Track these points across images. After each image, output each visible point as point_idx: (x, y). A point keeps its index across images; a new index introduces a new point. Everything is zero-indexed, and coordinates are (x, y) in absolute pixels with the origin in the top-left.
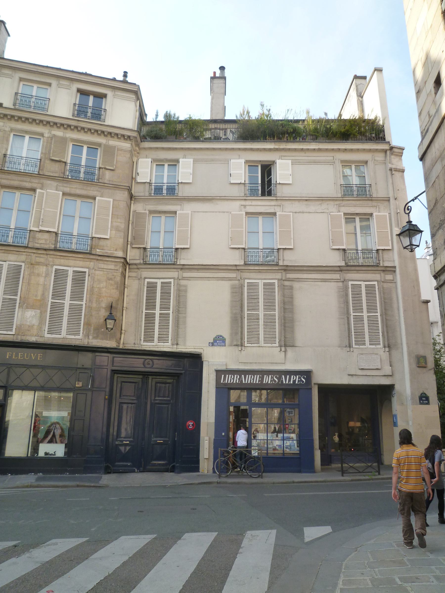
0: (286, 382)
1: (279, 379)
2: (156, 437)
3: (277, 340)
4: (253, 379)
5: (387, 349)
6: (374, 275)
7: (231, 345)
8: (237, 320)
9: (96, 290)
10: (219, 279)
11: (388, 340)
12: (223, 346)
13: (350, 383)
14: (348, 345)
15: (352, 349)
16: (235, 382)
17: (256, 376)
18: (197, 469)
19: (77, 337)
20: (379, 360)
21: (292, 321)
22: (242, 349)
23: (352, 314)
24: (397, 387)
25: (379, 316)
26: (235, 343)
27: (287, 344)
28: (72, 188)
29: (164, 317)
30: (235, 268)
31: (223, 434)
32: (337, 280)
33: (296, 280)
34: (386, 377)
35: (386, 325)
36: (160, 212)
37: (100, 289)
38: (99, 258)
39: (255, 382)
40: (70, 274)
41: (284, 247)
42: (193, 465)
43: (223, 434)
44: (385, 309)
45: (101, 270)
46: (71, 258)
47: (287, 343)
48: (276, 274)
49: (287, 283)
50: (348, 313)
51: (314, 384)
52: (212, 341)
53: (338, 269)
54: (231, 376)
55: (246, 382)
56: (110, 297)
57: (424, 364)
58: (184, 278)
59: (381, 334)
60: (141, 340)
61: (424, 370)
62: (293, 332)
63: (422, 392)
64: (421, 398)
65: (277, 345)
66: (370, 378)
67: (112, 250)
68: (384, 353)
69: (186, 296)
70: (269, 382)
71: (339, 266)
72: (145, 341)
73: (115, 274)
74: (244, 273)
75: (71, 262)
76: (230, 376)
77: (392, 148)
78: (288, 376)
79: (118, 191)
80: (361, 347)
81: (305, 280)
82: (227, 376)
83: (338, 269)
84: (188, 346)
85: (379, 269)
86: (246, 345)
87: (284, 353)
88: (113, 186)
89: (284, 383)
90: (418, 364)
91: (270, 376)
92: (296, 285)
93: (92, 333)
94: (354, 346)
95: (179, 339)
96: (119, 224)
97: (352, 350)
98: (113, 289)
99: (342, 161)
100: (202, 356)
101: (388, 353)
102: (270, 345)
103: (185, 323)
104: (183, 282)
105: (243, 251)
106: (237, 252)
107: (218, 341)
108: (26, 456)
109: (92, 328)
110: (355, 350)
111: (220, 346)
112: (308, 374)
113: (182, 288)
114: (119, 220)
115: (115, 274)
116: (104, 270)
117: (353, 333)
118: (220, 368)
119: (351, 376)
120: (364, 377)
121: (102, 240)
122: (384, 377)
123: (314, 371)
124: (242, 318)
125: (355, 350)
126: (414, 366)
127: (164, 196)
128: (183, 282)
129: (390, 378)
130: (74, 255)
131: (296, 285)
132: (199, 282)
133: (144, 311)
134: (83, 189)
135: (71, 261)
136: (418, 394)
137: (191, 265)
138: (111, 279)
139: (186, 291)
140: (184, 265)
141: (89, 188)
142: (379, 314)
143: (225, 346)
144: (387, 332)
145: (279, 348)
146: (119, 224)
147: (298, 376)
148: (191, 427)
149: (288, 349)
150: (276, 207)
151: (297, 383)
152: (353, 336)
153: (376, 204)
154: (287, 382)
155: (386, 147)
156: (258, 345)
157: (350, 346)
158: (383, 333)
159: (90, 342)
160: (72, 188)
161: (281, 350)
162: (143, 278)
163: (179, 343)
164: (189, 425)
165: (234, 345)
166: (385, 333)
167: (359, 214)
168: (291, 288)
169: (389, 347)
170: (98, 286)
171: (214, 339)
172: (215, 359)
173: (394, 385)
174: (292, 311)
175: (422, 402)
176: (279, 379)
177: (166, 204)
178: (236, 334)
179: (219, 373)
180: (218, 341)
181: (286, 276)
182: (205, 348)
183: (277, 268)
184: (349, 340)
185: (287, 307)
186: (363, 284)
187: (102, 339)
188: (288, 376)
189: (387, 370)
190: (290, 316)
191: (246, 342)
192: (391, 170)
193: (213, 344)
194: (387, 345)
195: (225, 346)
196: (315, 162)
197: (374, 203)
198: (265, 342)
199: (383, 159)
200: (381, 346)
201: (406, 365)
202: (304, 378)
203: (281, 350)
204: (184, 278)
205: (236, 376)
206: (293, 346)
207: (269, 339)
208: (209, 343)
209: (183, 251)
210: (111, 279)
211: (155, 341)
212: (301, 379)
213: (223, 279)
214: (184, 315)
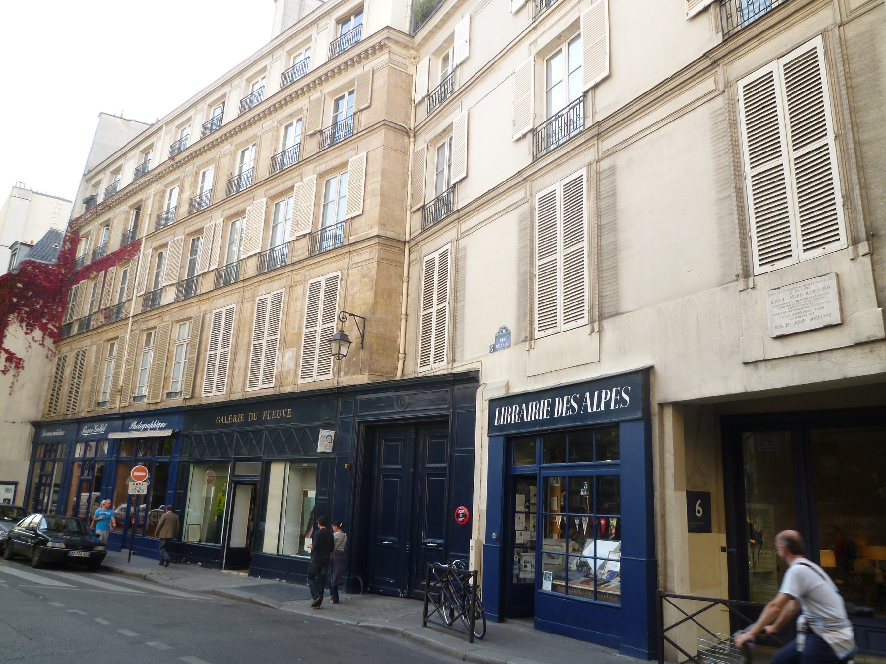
0: (592, 409)
1: (580, 402)
2: (429, 537)
6: (811, 20)
13: (749, 390)
21: (615, 250)
34: (867, 349)
38: (352, 249)
41: (592, 84)
50: (738, 174)
51: (662, 406)
53: (707, 62)
66: (812, 362)
68: (852, 264)
75: (318, 270)
78: (596, 393)
79: (374, 136)
80: (778, 265)
83: (707, 62)
91: (565, 398)
94: (758, 270)
108: (275, 553)
119: (751, 367)
121: (356, 219)
122: (859, 351)
123: (657, 368)
147: (614, 390)
148: (462, 519)
151: (612, 407)
152: (755, 240)
154: (594, 410)
157: (747, 273)
173: (478, 372)
176: (580, 402)
187: (354, 374)
188: (596, 393)
193: (494, 349)
202: (626, 392)
203: (592, 331)
206: (617, 314)
212: (621, 396)
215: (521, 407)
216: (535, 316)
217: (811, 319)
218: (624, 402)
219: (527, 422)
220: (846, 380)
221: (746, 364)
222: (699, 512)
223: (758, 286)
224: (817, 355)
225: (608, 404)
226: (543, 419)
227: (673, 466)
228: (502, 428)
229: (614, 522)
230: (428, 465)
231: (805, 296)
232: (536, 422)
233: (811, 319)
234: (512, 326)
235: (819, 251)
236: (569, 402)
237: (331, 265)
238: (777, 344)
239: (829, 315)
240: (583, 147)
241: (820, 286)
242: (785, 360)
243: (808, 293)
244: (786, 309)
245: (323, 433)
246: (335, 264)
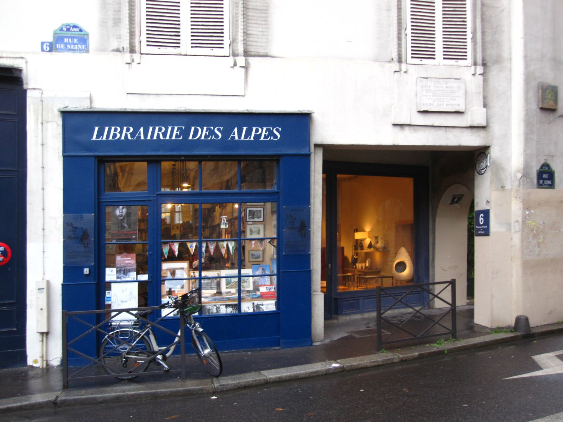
5: (480, 69)
7: (102, 50)
11: (484, 50)
12: (81, 51)
14: (395, 57)
15: (404, 67)
20: (462, 92)
22: (133, 61)
24: (494, 153)
31: (86, 271)
34: (474, 130)
35: (483, 15)
43: (86, 271)
51: (316, 146)
52: (50, 39)
57: (552, 103)
59: (469, 36)
61: (551, 116)
63: (542, 162)
64: (540, 175)
65: (226, 51)
66: (441, 132)
68: (473, 77)
82: (107, 128)
90: (543, 102)
97: (404, 69)
100: (24, 75)
101: (481, 77)
102: (208, 51)
107: (69, 38)
111: (74, 50)
112: (487, 233)
118: (73, 106)
119: (398, 128)
120: (428, 130)
123: (315, 116)
129: (482, 133)
136: (535, 168)
143: (88, 51)
144: (483, 33)
149: (251, 60)
152: (409, 38)
158: (474, 32)
161: (235, 64)
165: (113, 50)
166: (479, 34)
169: (484, 65)
171: (55, 34)
175: (541, 182)
176: (227, 132)
179: (76, 122)
180: (69, 38)
184: (399, 45)
189: (477, 116)
193: (52, 48)
194: (479, 61)
195: (88, 51)
196: (95, 205)
198: (195, 44)
203: (235, 64)
208: (43, 43)
217: (447, 105)
219: (145, 141)
220: (460, 147)
221: (395, 125)
222: (481, 221)
223: (409, 72)
224: (444, 128)
226: (170, 141)
227: (321, 196)
231: (445, 89)
233: (447, 105)
234: (91, 25)
235: (453, 62)
238: (421, 116)
239: (459, 105)
242: (423, 128)
243: (447, 87)
244: (431, 94)
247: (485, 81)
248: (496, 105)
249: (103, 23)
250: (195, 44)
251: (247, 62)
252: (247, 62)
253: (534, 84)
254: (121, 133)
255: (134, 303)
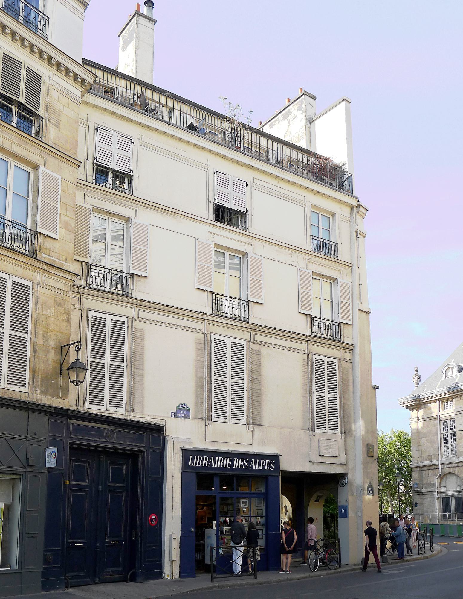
0: (256, 467)
1: (249, 463)
3: (245, 417)
4: (223, 463)
7: (195, 418)
8: (203, 385)
9: (42, 318)
10: (183, 328)
12: (187, 418)
16: (203, 465)
17: (226, 458)
18: (159, 575)
19: (22, 389)
20: (336, 447)
21: (259, 394)
23: (315, 393)
24: (350, 476)
25: (338, 399)
26: (200, 416)
27: (254, 423)
28: (6, 138)
29: (117, 372)
30: (202, 317)
32: (303, 352)
33: (264, 344)
34: (341, 465)
36: (107, 212)
37: (47, 317)
39: (224, 466)
40: (9, 286)
42: (155, 570)
44: (343, 392)
45: (47, 287)
46: (9, 260)
47: (254, 421)
48: (245, 333)
49: (255, 347)
50: (312, 393)
54: (200, 458)
55: (216, 466)
56: (60, 332)
58: (140, 319)
59: (339, 419)
60: (86, 400)
62: (260, 408)
65: (245, 422)
66: (328, 466)
67: (61, 258)
69: (142, 346)
70: (227, 466)
71: (307, 336)
72: (91, 402)
73: (65, 297)
74: (210, 326)
76: (220, 458)
77: (359, 205)
78: (258, 460)
81: (273, 346)
82: (196, 457)
83: (305, 338)
84: (147, 414)
85: (341, 345)
86: (214, 419)
87: (251, 432)
88: (61, 154)
89: (254, 468)
92: (264, 350)
93: (39, 384)
94: (316, 430)
95: (136, 404)
96: (68, 219)
98: (63, 320)
99: (314, 206)
103: (142, 383)
104: (139, 325)
105: (209, 295)
106: (204, 294)
107: (182, 411)
109: (40, 376)
110: (317, 434)
112: (275, 458)
113: (139, 333)
114: (68, 213)
115: (65, 297)
116: (52, 289)
117: (315, 416)
122: (339, 466)
124: (209, 384)
125: (317, 434)
126: (366, 455)
127: (107, 187)
128: (139, 325)
129: (344, 467)
130: (14, 256)
131: (264, 350)
132: (159, 328)
133: (125, 364)
134: (22, 147)
135: (9, 264)
137: (151, 302)
138: (59, 304)
139: (143, 338)
140: (142, 300)
141: (28, 147)
142: (338, 396)
145: (246, 427)
146: (68, 219)
150: (246, 245)
153: (340, 268)
155: (354, 203)
156: (226, 420)
159: (38, 398)
160: (6, 138)
162: (85, 308)
163: (135, 410)
164: (152, 519)
167: (324, 276)
168: (259, 353)
170: (44, 313)
172: (183, 435)
174: (259, 383)
176: (249, 463)
177: (114, 202)
178: (202, 403)
179: (187, 453)
180: (182, 411)
181: (254, 338)
182: (167, 419)
183: (246, 325)
185: (255, 376)
186: (326, 360)
187: (53, 395)
188: (258, 460)
190: (258, 388)
191: (213, 416)
192: (357, 232)
197: (338, 266)
198: (233, 418)
199: (349, 215)
200: (339, 432)
201: (359, 453)
202: (273, 463)
204: (140, 319)
205: (205, 457)
207: (238, 414)
208: (172, 413)
209: (139, 279)
210: (59, 304)
211: (105, 404)
213: (187, 328)
214: (141, 372)
215: (210, 459)
216: (209, 404)
218: (272, 468)
225: (264, 467)
228: (193, 468)
229: (228, 520)
230: (109, 484)
232: (221, 468)
234: (191, 405)
235: (332, 432)
236: (242, 461)
237: (17, 268)
240: (244, 329)
241: (334, 443)
245: (49, 450)
246: (21, 270)
247: (345, 441)
248: (350, 452)
249: (196, 404)
250: (233, 418)
251: (253, 428)
252: (253, 428)
253: (366, 444)
254: (202, 461)
255: (258, 541)
